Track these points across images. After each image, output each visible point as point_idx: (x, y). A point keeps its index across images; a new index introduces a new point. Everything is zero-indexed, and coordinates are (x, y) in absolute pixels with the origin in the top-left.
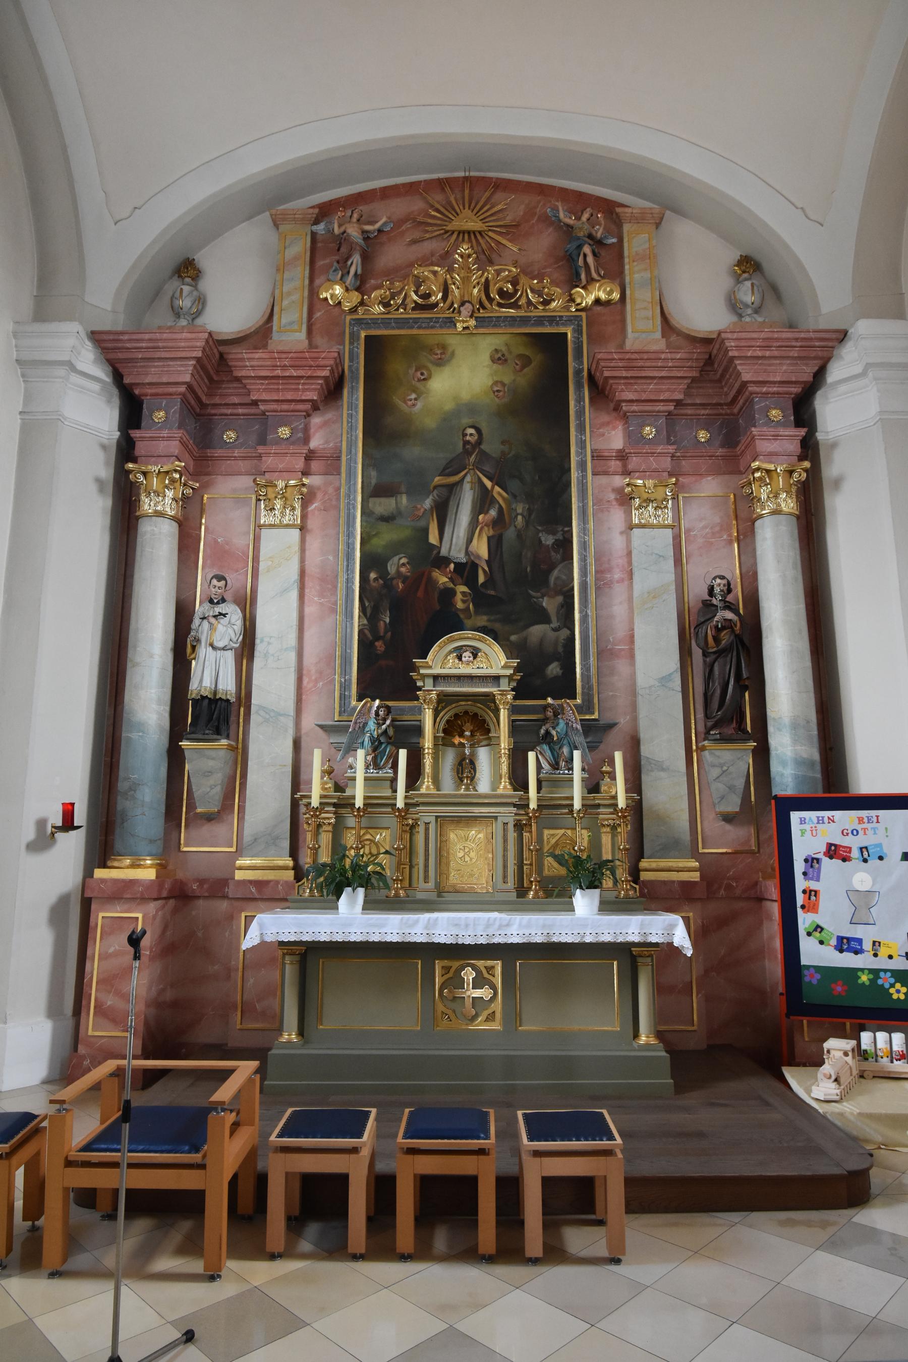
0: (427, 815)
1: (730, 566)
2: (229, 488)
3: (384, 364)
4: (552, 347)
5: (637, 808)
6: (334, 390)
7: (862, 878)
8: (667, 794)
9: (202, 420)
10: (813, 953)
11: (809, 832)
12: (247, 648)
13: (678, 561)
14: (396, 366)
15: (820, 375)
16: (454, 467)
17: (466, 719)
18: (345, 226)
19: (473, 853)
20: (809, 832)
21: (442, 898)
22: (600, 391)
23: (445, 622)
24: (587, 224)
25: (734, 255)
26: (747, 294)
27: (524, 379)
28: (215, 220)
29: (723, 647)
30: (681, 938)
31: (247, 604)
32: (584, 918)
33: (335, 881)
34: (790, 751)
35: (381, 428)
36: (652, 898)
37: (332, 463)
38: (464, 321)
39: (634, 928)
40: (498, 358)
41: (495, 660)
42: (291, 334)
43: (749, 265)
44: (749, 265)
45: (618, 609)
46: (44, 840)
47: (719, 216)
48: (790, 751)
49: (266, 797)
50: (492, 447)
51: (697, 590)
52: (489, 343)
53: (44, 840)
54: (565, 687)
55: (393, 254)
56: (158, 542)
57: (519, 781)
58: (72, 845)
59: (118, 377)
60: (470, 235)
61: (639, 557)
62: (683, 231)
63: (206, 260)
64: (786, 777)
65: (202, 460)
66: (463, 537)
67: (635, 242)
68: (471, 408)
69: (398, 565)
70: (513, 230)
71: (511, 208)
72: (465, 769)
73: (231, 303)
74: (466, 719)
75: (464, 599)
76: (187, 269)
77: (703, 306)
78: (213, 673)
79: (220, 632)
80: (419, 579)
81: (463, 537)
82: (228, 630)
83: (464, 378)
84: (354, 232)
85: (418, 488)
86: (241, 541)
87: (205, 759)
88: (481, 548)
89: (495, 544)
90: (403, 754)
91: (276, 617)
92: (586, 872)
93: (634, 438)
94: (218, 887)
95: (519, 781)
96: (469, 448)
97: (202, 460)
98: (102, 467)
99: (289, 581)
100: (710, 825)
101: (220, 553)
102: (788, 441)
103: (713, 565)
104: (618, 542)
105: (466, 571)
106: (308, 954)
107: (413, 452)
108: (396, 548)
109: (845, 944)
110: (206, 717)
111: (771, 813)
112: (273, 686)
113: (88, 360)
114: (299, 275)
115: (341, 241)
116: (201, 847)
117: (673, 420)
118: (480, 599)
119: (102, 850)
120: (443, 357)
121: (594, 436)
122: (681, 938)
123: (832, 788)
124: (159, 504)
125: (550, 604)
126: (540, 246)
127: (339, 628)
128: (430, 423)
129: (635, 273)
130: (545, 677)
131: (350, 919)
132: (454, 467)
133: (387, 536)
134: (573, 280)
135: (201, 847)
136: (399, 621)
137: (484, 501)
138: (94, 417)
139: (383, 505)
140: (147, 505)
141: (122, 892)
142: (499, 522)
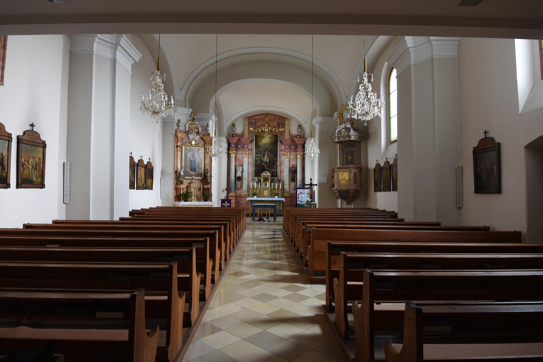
0: (262, 189)
1: (294, 163)
2: (240, 152)
3: (258, 138)
4: (276, 137)
5: (283, 188)
6: (251, 142)
7: (303, 196)
8: (287, 187)
9: (236, 145)
10: (298, 202)
11: (299, 191)
12: (242, 172)
13: (289, 162)
14: (259, 139)
15: (305, 143)
16: (265, 151)
17: (266, 179)
18: (252, 120)
19: (266, 193)
20: (299, 191)
21: (263, 197)
22: (281, 142)
23: (264, 170)
24: (280, 120)
25: (298, 124)
26: (299, 130)
27: (273, 140)
28: (237, 119)
29: (293, 172)
30: (284, 200)
31: (242, 166)
32: (276, 198)
33: (254, 195)
34: (299, 183)
35: (257, 146)
36: (283, 197)
37: (252, 150)
38: (266, 133)
39: (280, 199)
40: (270, 138)
41: (269, 174)
42: (246, 134)
43: (300, 126)
44: (300, 126)
45: (283, 167)
46: (223, 191)
47: (296, 120)
48: (299, 183)
49: (245, 187)
50: (269, 149)
51: (291, 165)
52: (269, 136)
53: (223, 191)
54: (276, 176)
55: (258, 124)
56: (233, 160)
57: (271, 186)
58: (226, 192)
59: (228, 141)
60: (267, 122)
61: (285, 161)
62: (293, 121)
63: (236, 124)
64: (298, 186)
65: (237, 149)
66: (266, 159)
67: (287, 123)
68: (267, 144)
69: (259, 162)
70: (272, 121)
71: (272, 118)
72: (266, 184)
73: (239, 130)
74: (266, 179)
75: (265, 167)
76: (234, 125)
77: (294, 131)
78: (239, 174)
79: (239, 170)
80: (261, 164)
81: (266, 159)
82: (241, 170)
83: (266, 140)
84: (254, 122)
85: (261, 153)
86: (241, 159)
87: (239, 183)
88: (268, 160)
89: (269, 160)
90: (308, 225)
91: (245, 167)
92: (277, 195)
93: (285, 148)
94: (240, 196)
95: (271, 186)
96: (267, 149)
97: (237, 149)
98: (226, 151)
99: (247, 162)
100: (291, 190)
101: (239, 160)
102: (301, 150)
103: (293, 163)
104: (283, 160)
105: (266, 163)
106: (251, 201)
107: (260, 149)
108: (259, 160)
109: (301, 202)
110: (239, 179)
111: (296, 189)
112: (245, 175)
113: (225, 140)
114: (247, 127)
115: (252, 123)
116: (239, 192)
117: (290, 148)
118: (267, 166)
119: (228, 192)
120: (264, 137)
121: (280, 147)
122: (284, 200)
123: (303, 186)
124: (233, 156)
125: (275, 167)
126: (275, 123)
127: (252, 169)
128: (262, 145)
129: (286, 127)
130: (274, 175)
131: (255, 198)
132: (265, 151)
133: (257, 159)
134: (279, 128)
135: (239, 192)
136: (259, 169)
137: (268, 155)
138: (225, 145)
139: (257, 155)
140: (232, 156)
141: (232, 196)
142: (270, 157)
